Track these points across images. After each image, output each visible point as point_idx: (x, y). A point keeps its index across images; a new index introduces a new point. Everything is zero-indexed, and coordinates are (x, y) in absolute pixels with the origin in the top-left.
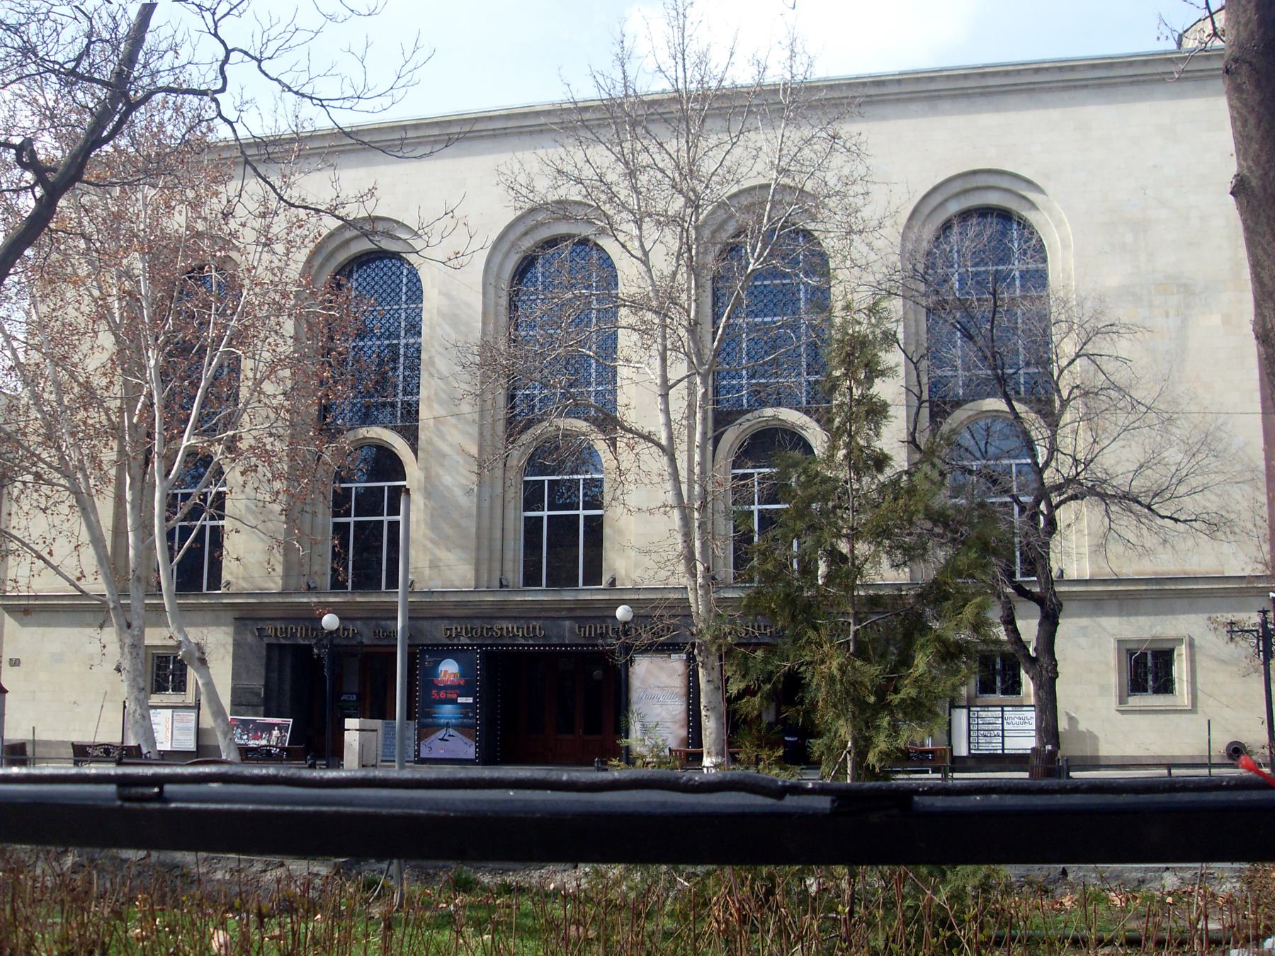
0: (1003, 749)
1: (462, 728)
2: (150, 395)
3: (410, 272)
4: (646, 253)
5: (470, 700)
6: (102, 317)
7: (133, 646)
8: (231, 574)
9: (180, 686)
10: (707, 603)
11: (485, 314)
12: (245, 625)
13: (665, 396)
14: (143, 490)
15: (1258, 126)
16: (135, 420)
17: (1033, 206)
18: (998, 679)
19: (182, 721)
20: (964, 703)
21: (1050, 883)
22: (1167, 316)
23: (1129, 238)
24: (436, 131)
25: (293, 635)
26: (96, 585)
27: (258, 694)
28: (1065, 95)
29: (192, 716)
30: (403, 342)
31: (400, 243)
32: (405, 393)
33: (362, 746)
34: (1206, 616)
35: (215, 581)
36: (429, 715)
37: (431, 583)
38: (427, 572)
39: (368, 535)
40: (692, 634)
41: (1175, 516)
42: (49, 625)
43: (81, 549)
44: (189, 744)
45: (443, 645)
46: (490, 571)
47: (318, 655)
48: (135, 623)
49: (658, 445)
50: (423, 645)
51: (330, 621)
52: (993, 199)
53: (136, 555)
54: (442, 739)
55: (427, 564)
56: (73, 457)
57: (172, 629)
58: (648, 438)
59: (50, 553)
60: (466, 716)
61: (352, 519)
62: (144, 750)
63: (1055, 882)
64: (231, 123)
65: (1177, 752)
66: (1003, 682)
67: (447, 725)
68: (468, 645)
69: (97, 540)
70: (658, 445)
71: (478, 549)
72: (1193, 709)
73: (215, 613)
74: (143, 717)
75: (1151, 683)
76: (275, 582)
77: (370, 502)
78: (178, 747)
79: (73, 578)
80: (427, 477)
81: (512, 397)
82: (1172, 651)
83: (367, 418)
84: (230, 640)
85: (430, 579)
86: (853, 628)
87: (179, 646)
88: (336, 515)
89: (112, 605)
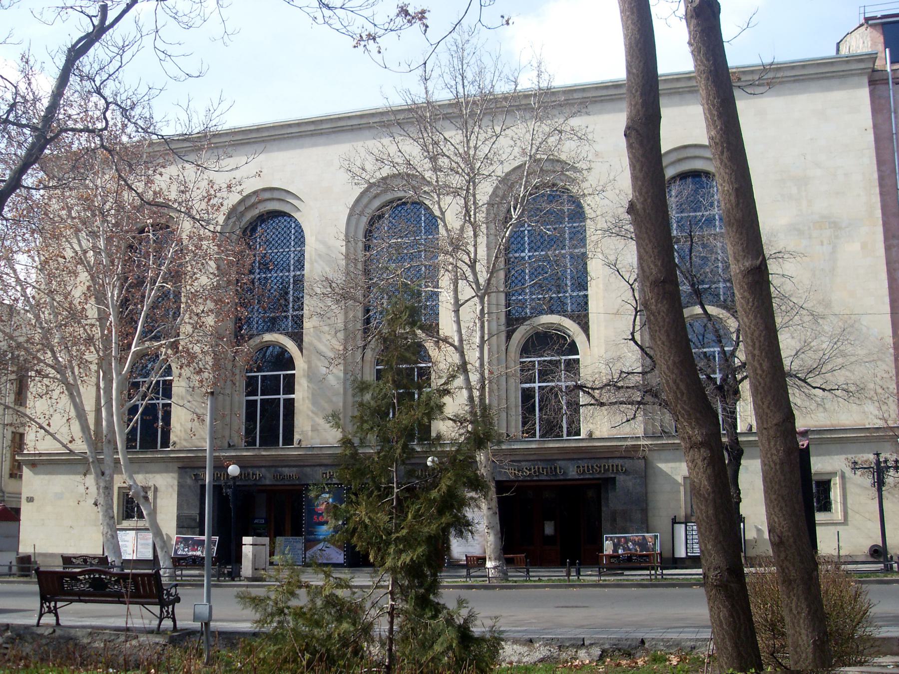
8: (177, 436)
12: (186, 472)
13: (457, 312)
14: (108, 382)
15: (641, 170)
19: (143, 539)
21: (632, 649)
22: (822, 244)
24: (312, 128)
26: (80, 446)
30: (292, 274)
31: (289, 205)
32: (294, 310)
34: (844, 456)
35: (166, 442)
36: (312, 533)
37: (313, 441)
38: (310, 433)
39: (270, 408)
41: (823, 387)
43: (72, 421)
48: (107, 472)
49: (452, 345)
55: (310, 428)
56: (62, 358)
59: (49, 425)
61: (259, 398)
63: (636, 648)
67: (324, 540)
70: (452, 345)
72: (845, 522)
73: (165, 464)
74: (113, 536)
78: (141, 557)
80: (309, 368)
82: (830, 481)
84: (176, 483)
86: (396, 490)
87: (130, 488)
89: (91, 460)
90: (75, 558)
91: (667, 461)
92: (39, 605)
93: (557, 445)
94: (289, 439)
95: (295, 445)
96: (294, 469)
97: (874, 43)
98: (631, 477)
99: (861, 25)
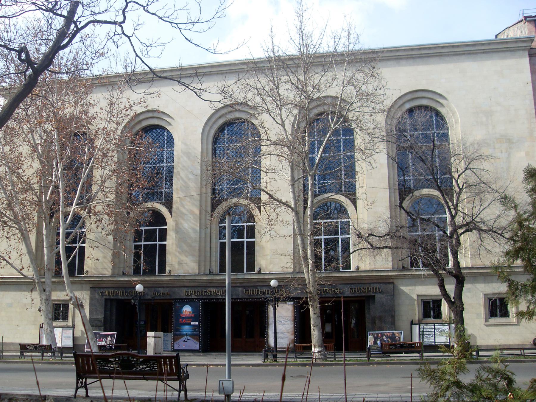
0: (435, 343)
1: (193, 336)
2: (57, 187)
3: (168, 135)
4: (283, 122)
5: (197, 323)
6: (35, 151)
7: (47, 300)
8: (88, 267)
9: (65, 318)
10: (314, 277)
11: (202, 152)
16: (48, 198)
17: (442, 105)
18: (432, 312)
19: (66, 333)
20: (417, 322)
23: (484, 119)
25: (117, 295)
26: (30, 272)
27: (101, 321)
28: (455, 58)
29: (71, 331)
30: (165, 165)
31: (164, 122)
33: (155, 345)
36: (178, 330)
40: (307, 292)
42: (5, 290)
43: (23, 256)
44: (70, 344)
45: (184, 299)
46: (205, 266)
47: (134, 303)
48: (47, 290)
50: (175, 299)
51: (139, 288)
52: (424, 102)
53: (48, 259)
54: (184, 341)
57: (68, 291)
58: (286, 204)
59: (10, 258)
60: (195, 331)
61: (143, 243)
62: (53, 347)
64: (129, 37)
65: (511, 343)
66: (434, 313)
67: (186, 335)
68: (196, 299)
69: (29, 252)
71: (200, 256)
74: (51, 332)
75: (499, 313)
76: (108, 271)
77: (150, 236)
79: (19, 269)
81: (214, 190)
83: (147, 198)
84: (88, 298)
85: (178, 270)
88: (135, 241)
90: (29, 345)
91: (407, 286)
92: (75, 381)
93: (338, 275)
94: (162, 270)
95: (167, 274)
96: (167, 289)
97: (530, 32)
98: (385, 295)
99: (522, 21)
